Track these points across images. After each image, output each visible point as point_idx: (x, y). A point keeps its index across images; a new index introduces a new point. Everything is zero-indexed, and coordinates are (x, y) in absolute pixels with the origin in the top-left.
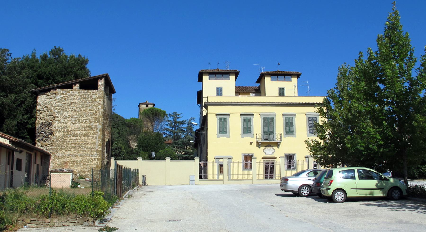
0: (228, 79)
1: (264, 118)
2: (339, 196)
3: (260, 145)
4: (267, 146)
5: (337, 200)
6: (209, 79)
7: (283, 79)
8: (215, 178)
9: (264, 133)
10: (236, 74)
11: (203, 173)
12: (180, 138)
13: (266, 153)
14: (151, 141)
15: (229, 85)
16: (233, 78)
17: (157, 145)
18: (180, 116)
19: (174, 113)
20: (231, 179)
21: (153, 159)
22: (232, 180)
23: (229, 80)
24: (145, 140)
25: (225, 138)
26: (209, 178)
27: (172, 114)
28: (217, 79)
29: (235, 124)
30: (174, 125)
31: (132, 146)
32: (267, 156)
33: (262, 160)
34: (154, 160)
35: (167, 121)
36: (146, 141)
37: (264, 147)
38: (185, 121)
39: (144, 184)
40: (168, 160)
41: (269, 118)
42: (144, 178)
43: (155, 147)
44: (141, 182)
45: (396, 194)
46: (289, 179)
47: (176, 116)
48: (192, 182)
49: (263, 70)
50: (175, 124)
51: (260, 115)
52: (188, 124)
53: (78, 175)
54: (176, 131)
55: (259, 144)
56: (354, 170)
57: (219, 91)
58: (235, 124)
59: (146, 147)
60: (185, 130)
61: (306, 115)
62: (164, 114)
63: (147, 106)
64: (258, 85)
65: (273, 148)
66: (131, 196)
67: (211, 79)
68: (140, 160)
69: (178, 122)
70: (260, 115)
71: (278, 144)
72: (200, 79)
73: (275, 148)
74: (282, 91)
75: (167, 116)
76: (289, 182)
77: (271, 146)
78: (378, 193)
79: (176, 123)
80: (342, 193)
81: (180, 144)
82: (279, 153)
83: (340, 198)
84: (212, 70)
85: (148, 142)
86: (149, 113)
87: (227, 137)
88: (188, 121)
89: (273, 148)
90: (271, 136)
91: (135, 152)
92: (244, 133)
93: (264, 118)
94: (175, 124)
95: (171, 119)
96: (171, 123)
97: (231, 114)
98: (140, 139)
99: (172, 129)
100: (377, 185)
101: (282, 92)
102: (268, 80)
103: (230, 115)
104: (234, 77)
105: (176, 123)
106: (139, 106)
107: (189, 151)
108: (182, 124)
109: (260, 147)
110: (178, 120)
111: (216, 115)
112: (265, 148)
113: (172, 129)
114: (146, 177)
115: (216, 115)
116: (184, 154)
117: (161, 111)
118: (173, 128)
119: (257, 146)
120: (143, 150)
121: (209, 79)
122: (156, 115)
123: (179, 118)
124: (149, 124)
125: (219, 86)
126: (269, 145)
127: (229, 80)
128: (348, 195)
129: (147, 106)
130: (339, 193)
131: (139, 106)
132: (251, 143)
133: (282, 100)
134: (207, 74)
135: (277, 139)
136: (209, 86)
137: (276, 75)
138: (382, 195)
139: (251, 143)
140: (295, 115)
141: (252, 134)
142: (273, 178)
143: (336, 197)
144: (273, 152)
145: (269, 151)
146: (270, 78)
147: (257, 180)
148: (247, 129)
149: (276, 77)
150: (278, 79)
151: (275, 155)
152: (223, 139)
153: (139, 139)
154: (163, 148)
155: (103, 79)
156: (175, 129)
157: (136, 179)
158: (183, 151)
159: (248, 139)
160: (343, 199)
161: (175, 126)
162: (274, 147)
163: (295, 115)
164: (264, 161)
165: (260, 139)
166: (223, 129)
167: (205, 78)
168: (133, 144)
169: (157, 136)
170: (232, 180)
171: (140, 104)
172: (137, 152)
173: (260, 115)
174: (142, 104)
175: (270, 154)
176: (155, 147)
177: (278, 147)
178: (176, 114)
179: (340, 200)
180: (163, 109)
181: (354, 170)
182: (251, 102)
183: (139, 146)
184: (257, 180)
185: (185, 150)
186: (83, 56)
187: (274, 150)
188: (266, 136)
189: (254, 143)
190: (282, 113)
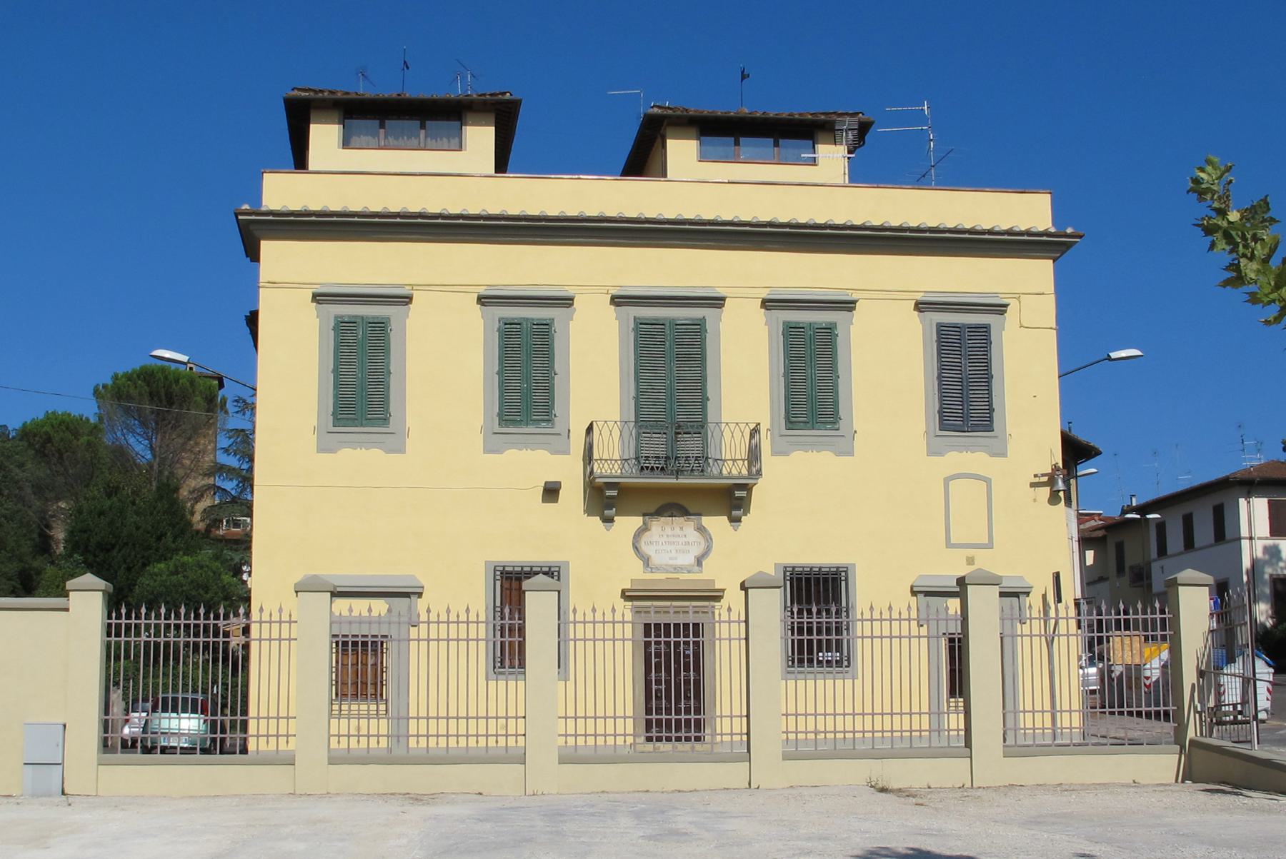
0: (455, 141)
4: (659, 513)
13: (656, 560)
17: (159, 538)
24: (101, 513)
29: (444, 359)
33: (625, 610)
37: (637, 521)
55: (605, 499)
58: (444, 359)
59: (106, 548)
65: (701, 529)
71: (732, 500)
73: (716, 524)
77: (685, 512)
85: (111, 523)
87: (389, 451)
89: (701, 529)
90: (689, 445)
92: (791, 423)
97: (416, 295)
109: (608, 520)
112: (644, 529)
119: (589, 511)
132: (551, 492)
139: (551, 492)
144: (697, 551)
145: (674, 547)
147: (334, 760)
152: (360, 459)
159: (533, 463)
162: (706, 521)
166: (362, 389)
176: (149, 547)
188: (657, 446)
189: (573, 492)
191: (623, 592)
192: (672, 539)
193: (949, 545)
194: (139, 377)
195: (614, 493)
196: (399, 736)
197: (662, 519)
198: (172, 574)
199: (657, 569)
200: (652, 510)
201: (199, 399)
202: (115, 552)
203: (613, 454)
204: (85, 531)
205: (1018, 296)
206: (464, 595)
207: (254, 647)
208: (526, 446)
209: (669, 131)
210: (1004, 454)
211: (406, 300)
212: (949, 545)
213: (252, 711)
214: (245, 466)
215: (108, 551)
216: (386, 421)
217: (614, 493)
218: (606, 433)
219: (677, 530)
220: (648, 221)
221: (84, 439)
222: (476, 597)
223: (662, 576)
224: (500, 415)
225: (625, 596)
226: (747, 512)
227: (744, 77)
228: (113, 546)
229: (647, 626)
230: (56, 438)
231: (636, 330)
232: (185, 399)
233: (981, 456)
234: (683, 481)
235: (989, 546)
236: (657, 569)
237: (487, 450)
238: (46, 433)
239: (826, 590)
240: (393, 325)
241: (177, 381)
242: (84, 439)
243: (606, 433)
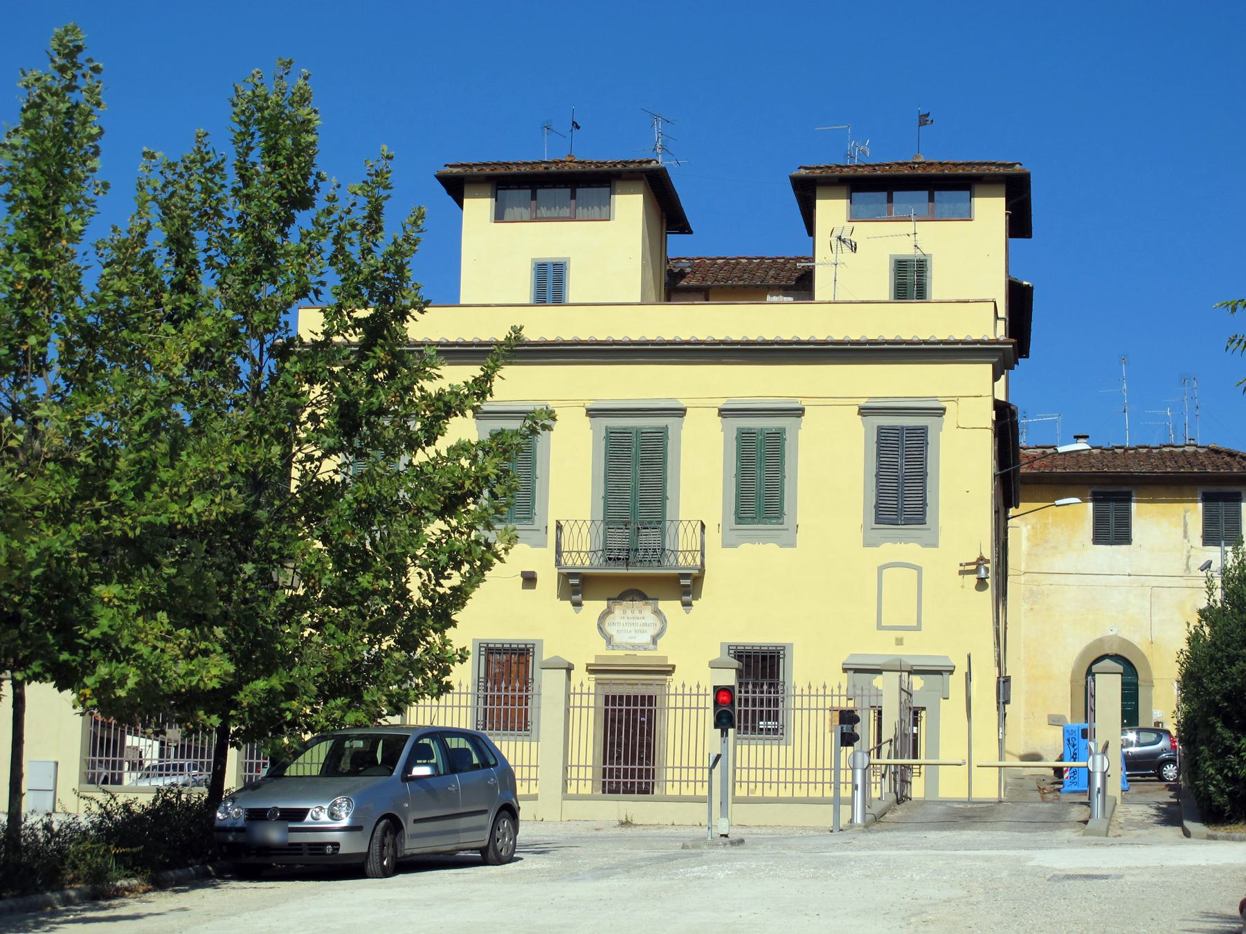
3: (575, 590)
4: (622, 597)
6: (499, 217)
7: (925, 206)
9: (609, 522)
13: (618, 638)
15: (609, 247)
22: (680, 799)
25: (772, 547)
28: (543, 212)
32: (618, 656)
37: (602, 605)
41: (640, 432)
55: (577, 586)
61: (864, 411)
65: (657, 612)
67: (509, 213)
70: (593, 413)
71: (686, 586)
73: (670, 607)
74: (912, 278)
77: (643, 597)
82: (690, 647)
84: (507, 165)
89: (657, 612)
90: (648, 539)
92: (740, 519)
93: (880, 428)
97: (949, 406)
101: (910, 281)
109: (577, 604)
112: (608, 612)
119: (562, 595)
121: (499, 217)
125: (906, 250)
126: (634, 591)
132: (529, 580)
133: (910, 323)
134: (488, 189)
135: (686, 562)
137: (876, 187)
139: (529, 580)
140: (799, 412)
141: (538, 523)
142: (646, 790)
144: (653, 631)
145: (633, 627)
149: (883, 195)
150: (895, 207)
151: (667, 651)
162: (663, 605)
163: (799, 412)
164: (599, 683)
166: (760, 492)
170: (680, 799)
175: (635, 647)
177: (687, 604)
187: (664, 621)
188: (620, 540)
189: (548, 579)
190: (721, 403)
191: (588, 665)
192: (631, 621)
193: (880, 627)
195: (576, 581)
197: (624, 603)
199: (618, 647)
200: (616, 596)
203: (583, 548)
205: (955, 399)
210: (935, 545)
212: (880, 627)
217: (576, 581)
219: (637, 614)
223: (621, 653)
224: (736, 513)
226: (697, 596)
229: (607, 697)
233: (914, 547)
234: (632, 571)
235: (918, 628)
236: (618, 647)
239: (764, 668)
240: (787, 436)
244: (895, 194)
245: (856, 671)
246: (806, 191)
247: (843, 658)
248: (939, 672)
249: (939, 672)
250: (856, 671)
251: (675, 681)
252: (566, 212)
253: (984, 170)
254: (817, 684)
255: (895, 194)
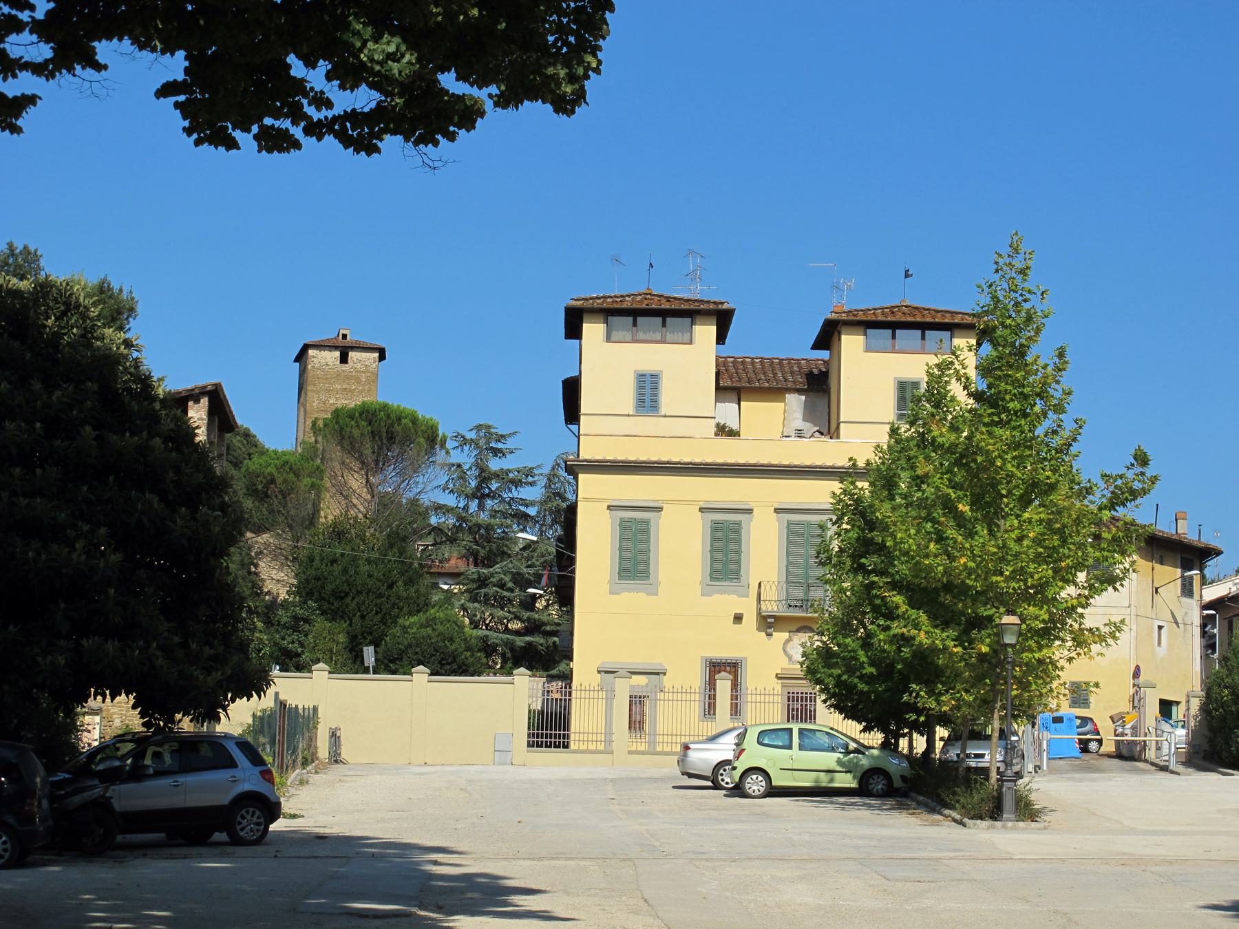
0: (687, 336)
1: (789, 523)
2: (755, 784)
3: (770, 626)
4: (798, 631)
5: (750, 791)
6: (608, 339)
8: (601, 747)
9: (789, 582)
10: (723, 320)
11: (550, 728)
12: (504, 555)
14: (365, 569)
15: (691, 360)
16: (706, 332)
17: (390, 587)
18: (509, 444)
19: (479, 428)
20: (659, 748)
21: (366, 671)
23: (691, 342)
24: (334, 561)
26: (573, 746)
27: (471, 435)
28: (641, 336)
29: (681, 543)
30: (478, 488)
31: (268, 586)
33: (778, 685)
34: (371, 676)
35: (443, 465)
36: (337, 568)
37: (786, 635)
38: (529, 472)
39: (336, 758)
40: (421, 674)
42: (334, 736)
43: (380, 596)
44: (323, 752)
45: (879, 785)
46: (692, 746)
47: (489, 442)
48: (502, 754)
49: (846, 303)
50: (483, 485)
51: (777, 511)
52: (548, 487)
53: (117, 723)
54: (484, 517)
55: (768, 623)
56: (790, 730)
57: (648, 393)
58: (681, 543)
59: (339, 595)
60: (532, 511)
62: (432, 439)
63: (344, 359)
64: (824, 355)
66: (307, 782)
67: (615, 335)
68: (321, 672)
69: (501, 475)
72: (573, 330)
75: (443, 445)
76: (690, 753)
78: (846, 781)
79: (485, 476)
80: (760, 778)
81: (502, 585)
83: (755, 788)
85: (345, 571)
86: (356, 432)
87: (649, 594)
88: (547, 470)
91: (284, 616)
92: (712, 578)
93: (789, 523)
94: (483, 485)
95: (465, 458)
96: (463, 477)
97: (665, 506)
98: (311, 560)
99: (466, 508)
100: (839, 762)
102: (851, 344)
103: (661, 509)
104: (712, 330)
105: (485, 476)
106: (301, 357)
107: (544, 618)
108: (517, 483)
109: (769, 635)
110: (495, 464)
111: (609, 507)
113: (466, 508)
114: (342, 734)
115: (609, 507)
116: (517, 633)
117: (414, 420)
118: (474, 505)
119: (759, 629)
120: (323, 613)
121: (608, 339)
122: (391, 438)
123: (496, 452)
124: (356, 482)
125: (648, 367)
127: (691, 342)
128: (776, 782)
129: (344, 359)
130: (754, 777)
131: (301, 357)
132: (738, 618)
136: (608, 361)
138: (853, 786)
139: (738, 618)
143: (748, 786)
146: (861, 338)
147: (630, 753)
148: (726, 563)
152: (633, 598)
153: (303, 555)
154: (421, 606)
155: (205, 401)
156: (481, 507)
157: (311, 739)
158: (517, 618)
159: (729, 601)
160: (762, 790)
161: (480, 495)
165: (772, 606)
166: (634, 563)
167: (593, 331)
168: (274, 574)
169: (391, 546)
171: (306, 348)
172: (296, 618)
173: (777, 511)
174: (319, 346)
176: (380, 596)
178: (489, 436)
179: (757, 793)
180: (424, 413)
181: (790, 730)
182: (741, 461)
183: (307, 589)
184: (630, 753)
185: (526, 615)
186: (116, 286)
188: (798, 593)
189: (750, 619)
194: (361, 415)
196: (652, 743)
198: (422, 626)
201: (421, 440)
202: (348, 600)
204: (319, 579)
206: (687, 676)
207: (573, 701)
208: (724, 592)
209: (843, 330)
211: (660, 509)
213: (572, 729)
214: (461, 505)
215: (342, 598)
216: (647, 577)
218: (768, 588)
220: (795, 466)
221: (307, 481)
222: (695, 678)
224: (711, 575)
225: (778, 677)
227: (907, 276)
228: (347, 595)
230: (279, 481)
231: (788, 528)
232: (407, 439)
237: (703, 595)
238: (270, 474)
240: (652, 523)
241: (399, 419)
242: (307, 481)
243: (768, 588)
244: (898, 331)
245: (606, 672)
246: (573, 324)
247: (597, 664)
248: (658, 674)
249: (658, 674)
250: (606, 672)
251: (666, 681)
252: (658, 336)
253: (589, 304)
254: (677, 686)
255: (898, 331)
